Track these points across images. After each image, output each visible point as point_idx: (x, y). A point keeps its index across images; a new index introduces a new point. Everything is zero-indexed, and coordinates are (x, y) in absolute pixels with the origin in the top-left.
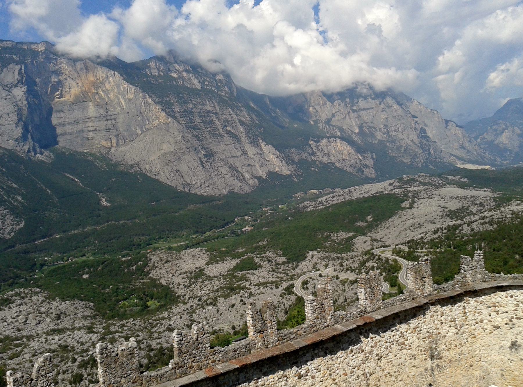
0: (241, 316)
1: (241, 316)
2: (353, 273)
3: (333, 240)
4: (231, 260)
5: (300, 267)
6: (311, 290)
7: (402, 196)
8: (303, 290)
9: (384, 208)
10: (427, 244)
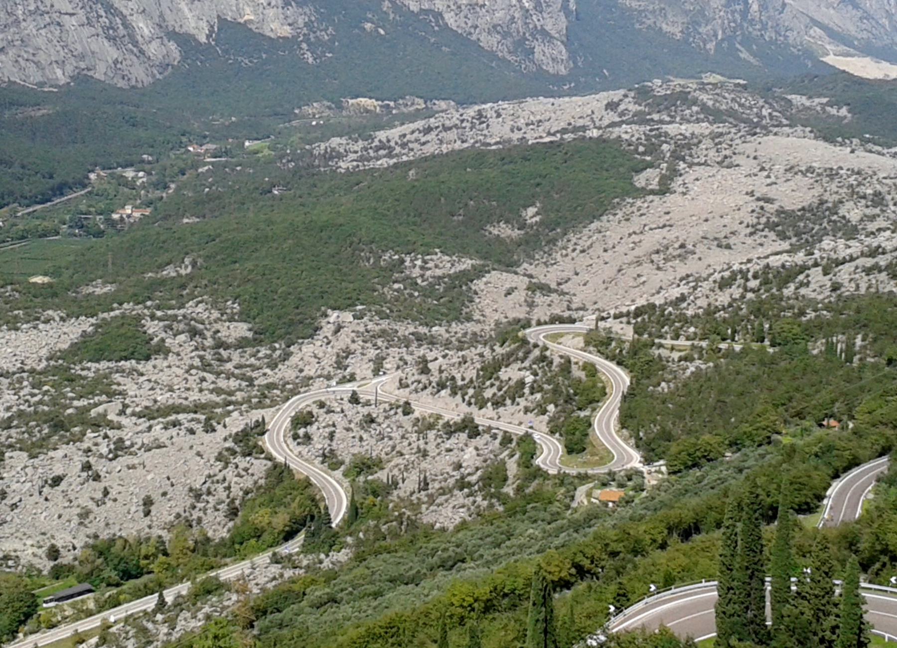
0: (80, 516)
1: (80, 516)
2: (459, 397)
3: (408, 277)
4: (62, 319)
5: (294, 360)
6: (319, 443)
7: (641, 149)
8: (292, 444)
9: (581, 183)
10: (692, 324)
